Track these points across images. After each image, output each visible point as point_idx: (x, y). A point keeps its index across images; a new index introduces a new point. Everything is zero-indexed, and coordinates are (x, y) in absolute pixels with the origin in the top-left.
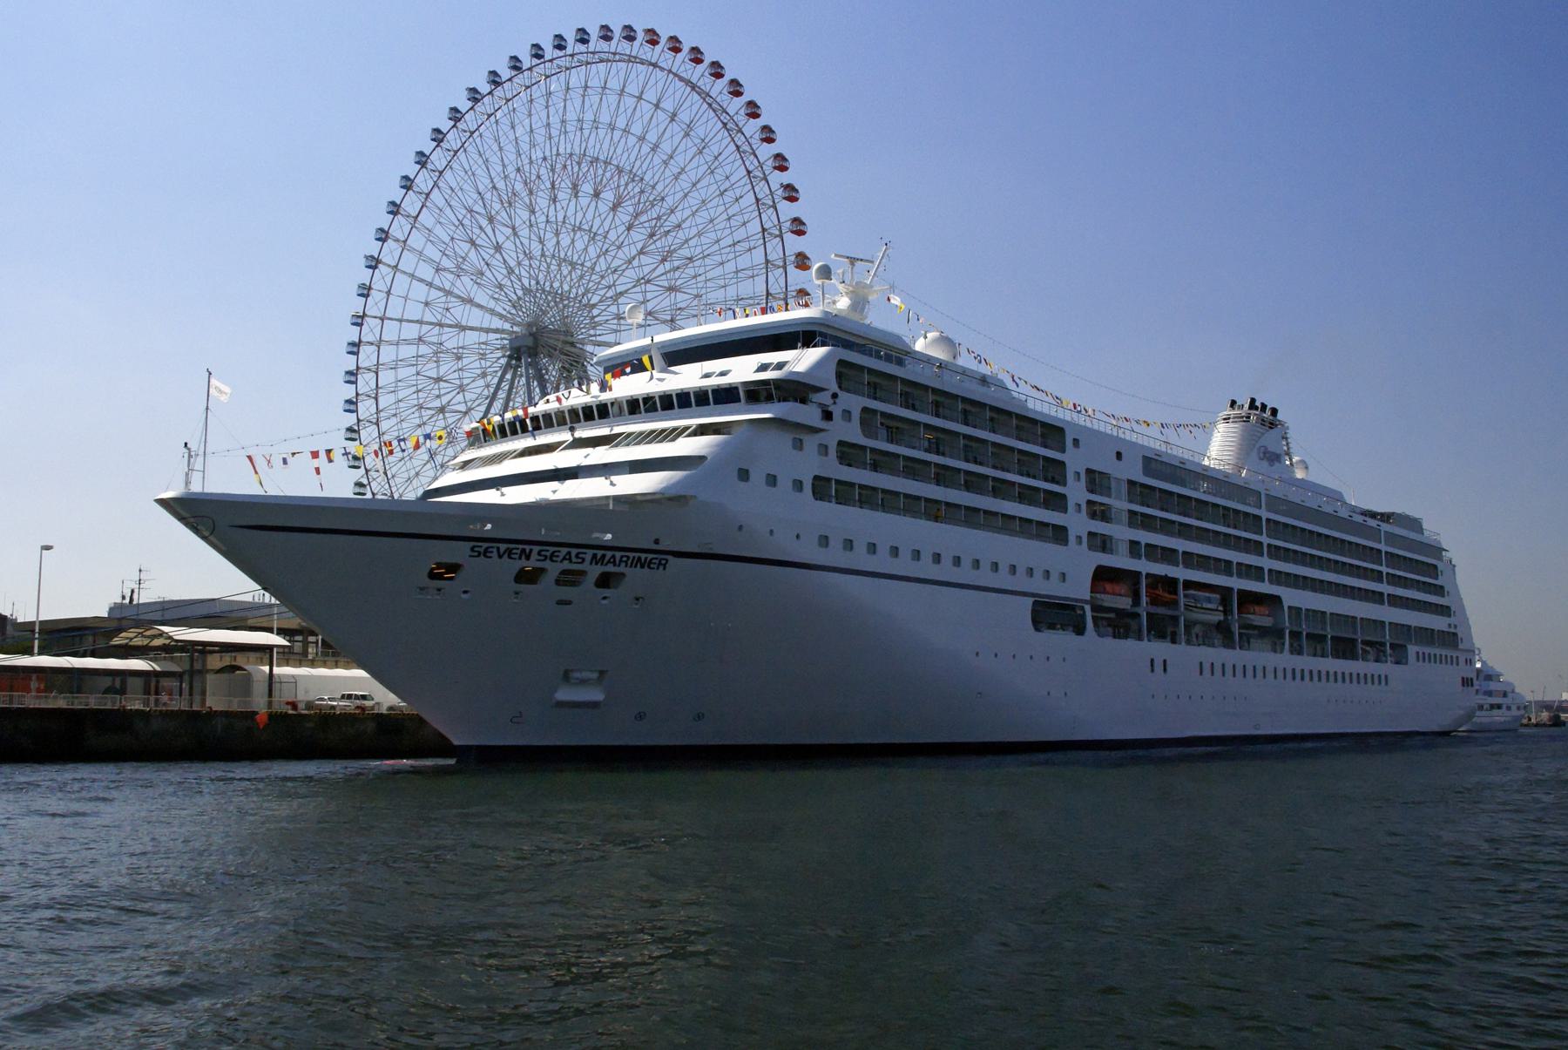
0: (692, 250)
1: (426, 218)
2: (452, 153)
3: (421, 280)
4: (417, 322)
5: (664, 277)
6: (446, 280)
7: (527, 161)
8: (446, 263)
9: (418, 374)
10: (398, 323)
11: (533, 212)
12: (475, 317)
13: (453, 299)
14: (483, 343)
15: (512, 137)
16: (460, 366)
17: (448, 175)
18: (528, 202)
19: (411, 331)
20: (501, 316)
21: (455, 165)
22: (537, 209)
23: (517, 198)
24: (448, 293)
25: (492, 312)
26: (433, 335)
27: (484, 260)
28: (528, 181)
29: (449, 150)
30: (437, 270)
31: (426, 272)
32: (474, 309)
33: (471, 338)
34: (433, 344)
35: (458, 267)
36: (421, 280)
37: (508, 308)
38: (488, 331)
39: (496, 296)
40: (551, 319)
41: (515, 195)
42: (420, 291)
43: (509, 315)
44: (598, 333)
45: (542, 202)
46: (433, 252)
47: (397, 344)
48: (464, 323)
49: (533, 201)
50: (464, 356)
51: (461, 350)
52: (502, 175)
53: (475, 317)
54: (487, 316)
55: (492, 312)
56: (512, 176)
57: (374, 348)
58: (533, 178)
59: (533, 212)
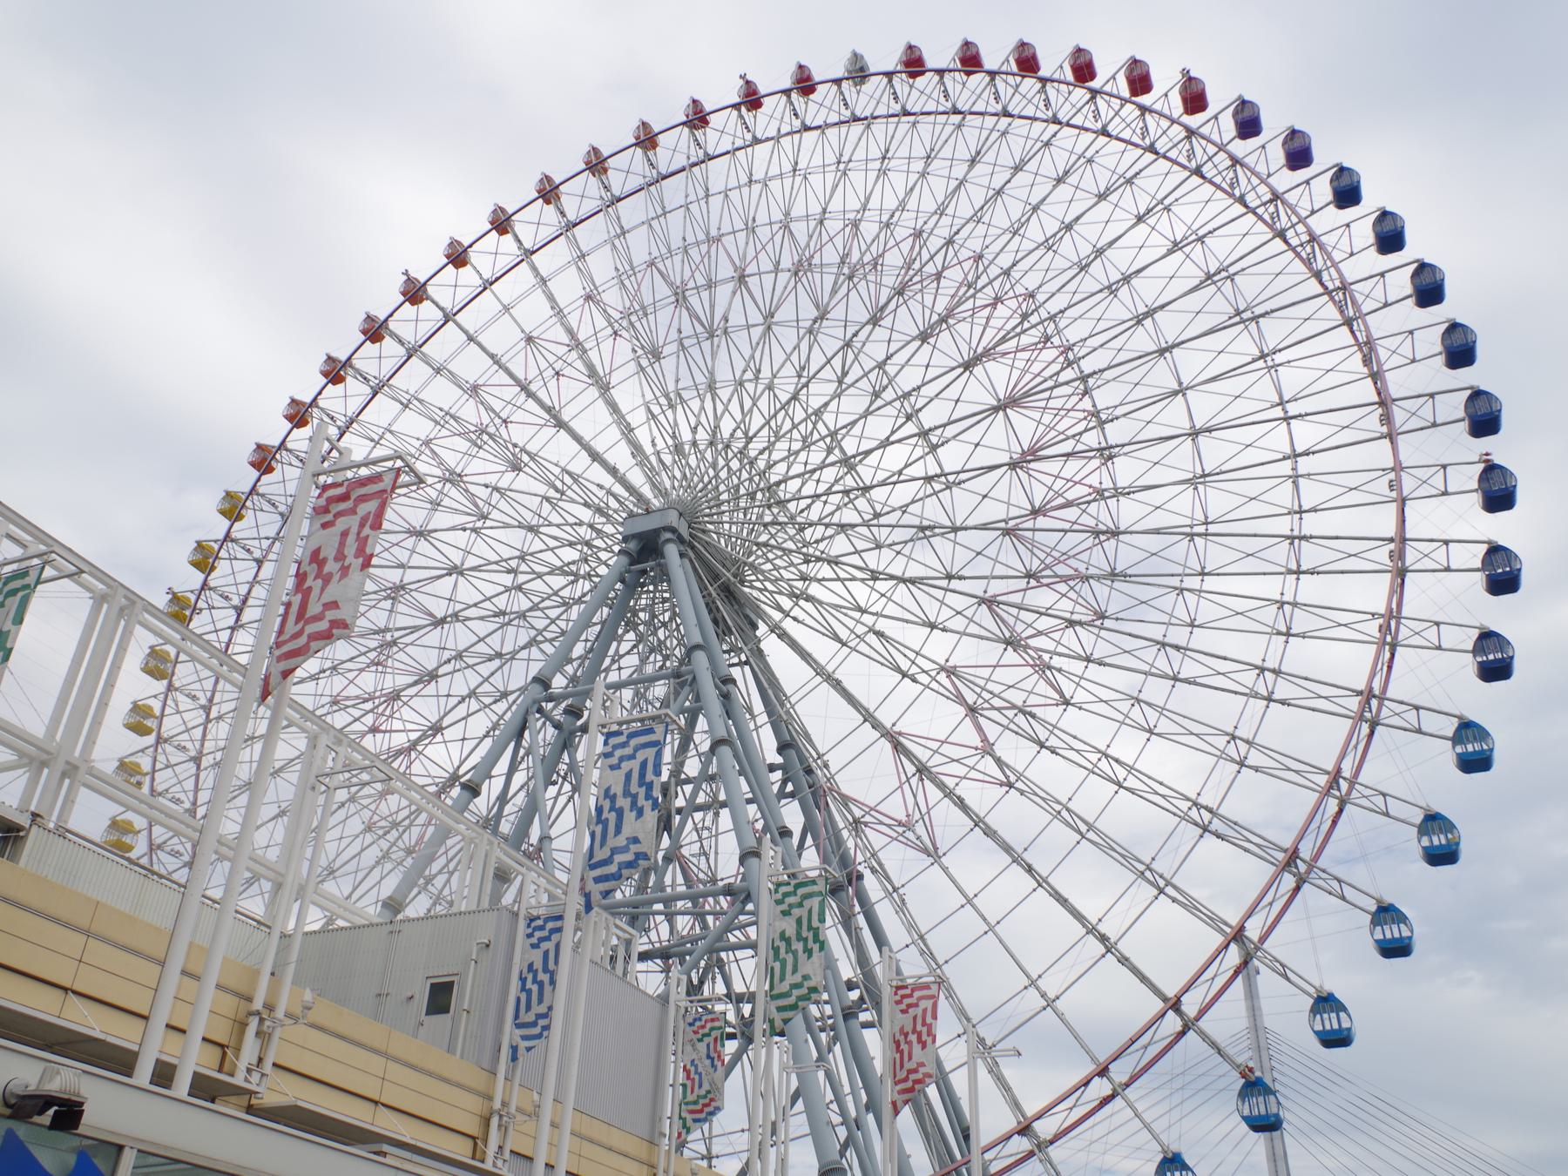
0: (991, 552)
1: (631, 211)
2: (896, 108)
3: (551, 298)
4: (492, 356)
5: (1014, 611)
6: (588, 323)
7: (945, 233)
8: (613, 298)
9: (427, 443)
10: (1409, 505)
11: (875, 321)
12: (593, 420)
13: (579, 364)
14: (528, 453)
15: (959, 171)
16: (503, 484)
17: (762, 150)
18: (883, 301)
19: (472, 365)
20: (637, 449)
21: (878, 128)
22: (887, 322)
23: (871, 277)
24: (576, 345)
25: (628, 431)
26: (502, 393)
27: (680, 331)
28: (917, 266)
29: (896, 99)
30: (589, 298)
31: (568, 288)
32: (601, 404)
33: (560, 449)
34: (489, 409)
35: (626, 314)
36: (551, 298)
37: (660, 445)
38: (595, 456)
39: (656, 409)
40: (725, 532)
41: (875, 267)
42: (534, 312)
43: (653, 459)
44: (796, 612)
45: (906, 321)
46: (602, 266)
47: (438, 371)
48: (565, 417)
49: (892, 305)
50: (526, 469)
51: (526, 458)
52: (885, 218)
53: (593, 420)
54: (614, 433)
55: (628, 431)
56: (901, 233)
57: (402, 351)
58: (930, 269)
59: (875, 321)
